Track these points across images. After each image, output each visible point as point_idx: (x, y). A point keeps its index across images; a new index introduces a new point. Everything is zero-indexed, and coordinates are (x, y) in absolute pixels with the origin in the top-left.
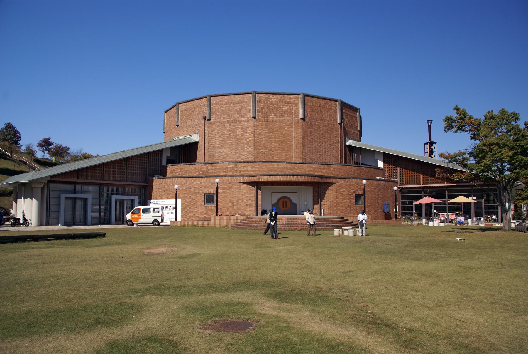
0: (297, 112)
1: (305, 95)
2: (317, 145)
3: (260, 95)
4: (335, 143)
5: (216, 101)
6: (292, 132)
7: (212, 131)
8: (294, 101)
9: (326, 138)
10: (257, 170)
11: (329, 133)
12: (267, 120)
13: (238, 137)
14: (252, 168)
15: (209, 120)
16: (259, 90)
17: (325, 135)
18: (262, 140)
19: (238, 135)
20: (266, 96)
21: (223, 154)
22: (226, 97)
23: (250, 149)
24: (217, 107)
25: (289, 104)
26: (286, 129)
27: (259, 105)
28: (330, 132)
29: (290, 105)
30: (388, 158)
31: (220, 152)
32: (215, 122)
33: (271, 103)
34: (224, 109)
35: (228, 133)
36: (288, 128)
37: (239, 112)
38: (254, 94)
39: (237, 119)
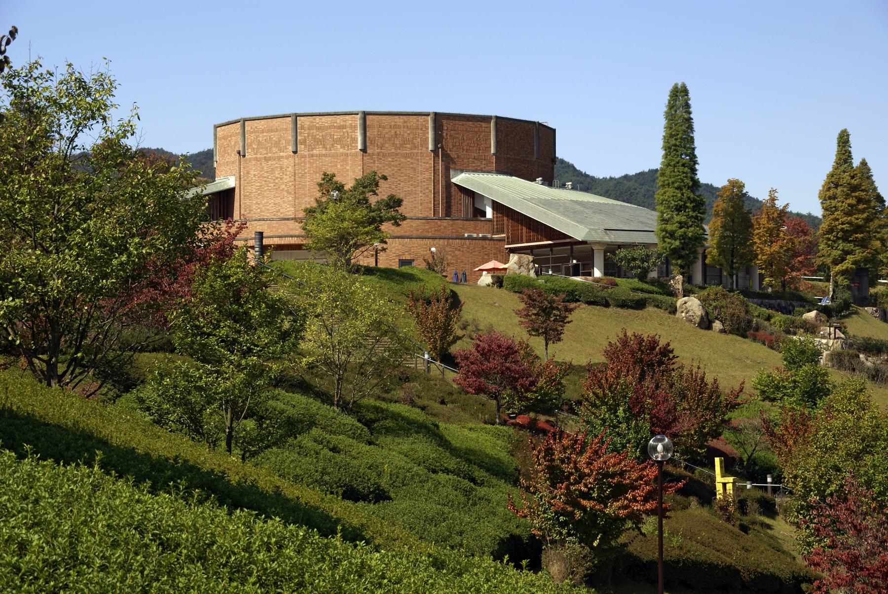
0: (354, 140)
1: (365, 114)
2: (390, 188)
3: (302, 118)
4: (424, 182)
5: (251, 128)
6: (347, 171)
7: (248, 173)
8: (351, 124)
9: (406, 176)
10: (274, 230)
11: (413, 168)
12: (312, 156)
13: (277, 181)
14: (269, 228)
15: (244, 156)
16: (299, 111)
17: (404, 171)
18: (305, 185)
19: (277, 178)
20: (311, 119)
21: (261, 206)
22: (263, 122)
23: (290, 199)
24: (253, 136)
25: (343, 128)
26: (339, 166)
27: (301, 133)
28: (414, 165)
29: (344, 130)
30: (497, 206)
31: (257, 203)
32: (250, 158)
33: (319, 129)
34: (261, 139)
35: (266, 175)
36: (341, 166)
37: (277, 144)
38: (294, 118)
39: (276, 155)
